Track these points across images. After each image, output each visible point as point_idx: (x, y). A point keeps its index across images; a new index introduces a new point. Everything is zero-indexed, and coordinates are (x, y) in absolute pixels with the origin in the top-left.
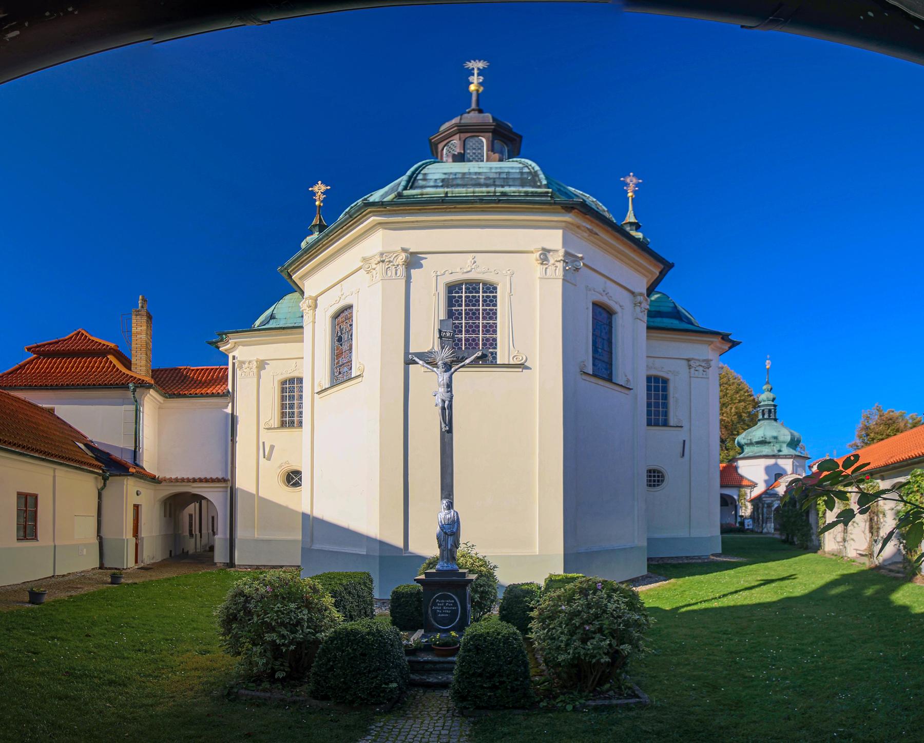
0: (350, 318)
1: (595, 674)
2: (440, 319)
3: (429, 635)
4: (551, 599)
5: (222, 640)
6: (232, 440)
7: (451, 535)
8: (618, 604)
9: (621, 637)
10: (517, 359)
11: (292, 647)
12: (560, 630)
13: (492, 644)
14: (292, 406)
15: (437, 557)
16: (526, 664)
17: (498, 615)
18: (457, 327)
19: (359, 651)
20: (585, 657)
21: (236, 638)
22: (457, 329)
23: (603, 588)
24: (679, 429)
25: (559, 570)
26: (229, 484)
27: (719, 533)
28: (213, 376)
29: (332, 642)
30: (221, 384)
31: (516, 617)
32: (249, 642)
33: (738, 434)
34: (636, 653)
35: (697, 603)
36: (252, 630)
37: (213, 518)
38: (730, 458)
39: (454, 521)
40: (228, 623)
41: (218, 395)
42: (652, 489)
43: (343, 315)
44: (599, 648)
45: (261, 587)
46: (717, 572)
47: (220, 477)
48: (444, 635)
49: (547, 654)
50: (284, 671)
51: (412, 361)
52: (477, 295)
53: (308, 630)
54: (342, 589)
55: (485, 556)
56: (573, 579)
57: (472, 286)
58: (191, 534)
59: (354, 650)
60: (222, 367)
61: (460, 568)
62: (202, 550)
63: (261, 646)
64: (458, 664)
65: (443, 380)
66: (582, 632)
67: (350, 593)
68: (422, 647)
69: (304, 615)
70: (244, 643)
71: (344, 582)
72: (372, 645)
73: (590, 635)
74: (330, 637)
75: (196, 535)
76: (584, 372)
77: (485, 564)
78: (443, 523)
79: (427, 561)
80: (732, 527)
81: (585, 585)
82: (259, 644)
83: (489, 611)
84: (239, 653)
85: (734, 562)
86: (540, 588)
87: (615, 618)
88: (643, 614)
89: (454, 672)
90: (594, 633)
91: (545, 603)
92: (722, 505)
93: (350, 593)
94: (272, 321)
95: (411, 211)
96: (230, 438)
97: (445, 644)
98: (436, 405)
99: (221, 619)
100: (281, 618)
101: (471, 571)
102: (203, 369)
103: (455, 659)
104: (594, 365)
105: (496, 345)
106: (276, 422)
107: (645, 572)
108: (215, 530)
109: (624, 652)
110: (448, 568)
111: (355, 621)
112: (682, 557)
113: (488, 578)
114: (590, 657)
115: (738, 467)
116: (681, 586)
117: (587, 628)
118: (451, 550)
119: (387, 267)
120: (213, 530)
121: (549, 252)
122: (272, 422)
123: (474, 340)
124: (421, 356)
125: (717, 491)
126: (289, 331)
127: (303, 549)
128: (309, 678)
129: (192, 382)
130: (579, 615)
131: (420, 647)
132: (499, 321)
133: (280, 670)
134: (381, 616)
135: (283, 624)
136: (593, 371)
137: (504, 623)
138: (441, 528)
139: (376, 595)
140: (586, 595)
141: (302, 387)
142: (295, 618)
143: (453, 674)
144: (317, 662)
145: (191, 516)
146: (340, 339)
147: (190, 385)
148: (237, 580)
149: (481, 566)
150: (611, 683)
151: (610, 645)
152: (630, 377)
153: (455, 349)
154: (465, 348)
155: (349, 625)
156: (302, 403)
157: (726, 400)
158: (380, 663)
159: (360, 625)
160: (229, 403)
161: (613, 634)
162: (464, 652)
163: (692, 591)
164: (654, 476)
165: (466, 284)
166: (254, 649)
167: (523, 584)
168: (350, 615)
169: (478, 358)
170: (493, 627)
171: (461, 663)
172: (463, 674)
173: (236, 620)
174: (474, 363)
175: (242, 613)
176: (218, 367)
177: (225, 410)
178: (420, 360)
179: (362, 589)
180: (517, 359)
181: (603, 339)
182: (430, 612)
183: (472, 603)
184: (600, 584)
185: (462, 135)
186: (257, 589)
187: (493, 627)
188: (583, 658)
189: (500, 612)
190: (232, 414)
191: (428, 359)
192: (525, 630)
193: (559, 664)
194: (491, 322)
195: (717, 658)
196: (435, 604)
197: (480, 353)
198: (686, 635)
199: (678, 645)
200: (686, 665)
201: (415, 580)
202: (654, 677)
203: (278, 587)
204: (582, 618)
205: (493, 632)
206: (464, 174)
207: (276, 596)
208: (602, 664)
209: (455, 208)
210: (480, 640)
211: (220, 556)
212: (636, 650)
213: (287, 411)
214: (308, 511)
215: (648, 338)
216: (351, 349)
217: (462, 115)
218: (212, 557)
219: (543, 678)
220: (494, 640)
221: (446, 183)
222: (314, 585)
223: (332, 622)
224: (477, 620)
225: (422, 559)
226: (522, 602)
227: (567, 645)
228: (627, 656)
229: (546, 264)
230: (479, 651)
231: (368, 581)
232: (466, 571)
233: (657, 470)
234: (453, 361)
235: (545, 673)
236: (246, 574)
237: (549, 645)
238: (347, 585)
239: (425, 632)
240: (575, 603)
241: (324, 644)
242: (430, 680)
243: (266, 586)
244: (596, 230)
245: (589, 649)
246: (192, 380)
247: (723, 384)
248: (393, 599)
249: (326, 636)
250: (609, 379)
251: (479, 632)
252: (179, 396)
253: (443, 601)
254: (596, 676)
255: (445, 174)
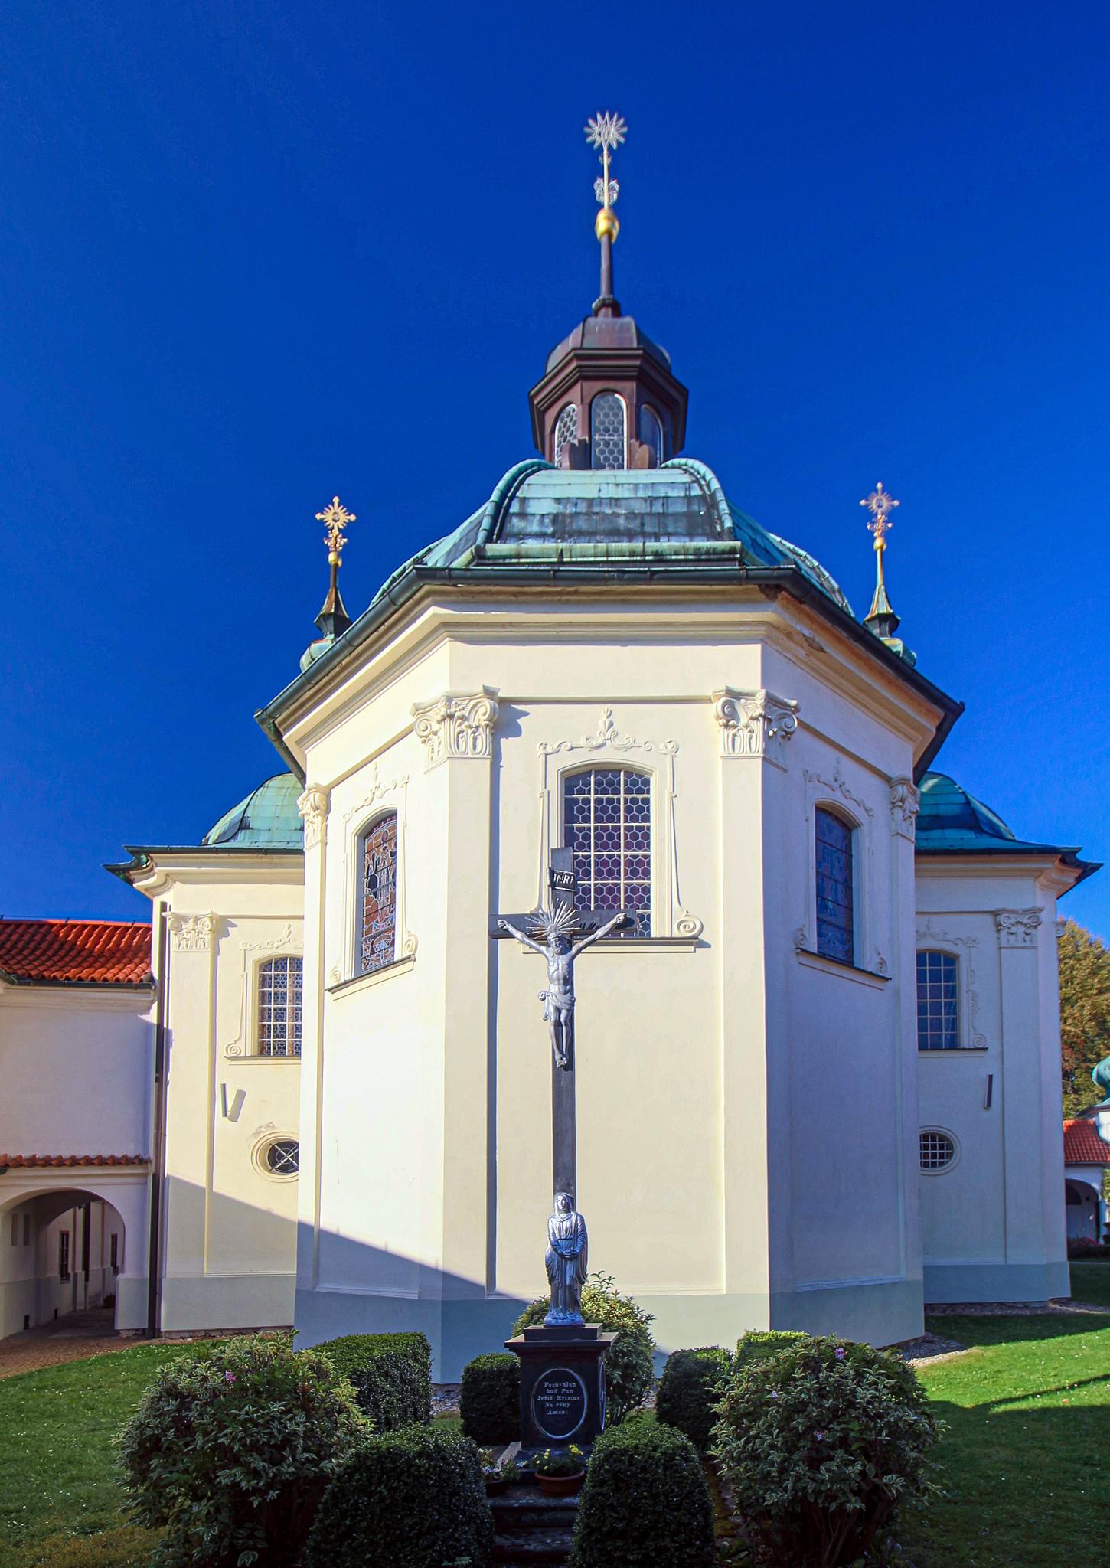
0: (390, 839)
1: (834, 1535)
2: (551, 847)
3: (530, 1453)
4: (752, 1377)
5: (128, 1497)
6: (157, 1080)
7: (571, 1259)
8: (877, 1389)
9: (882, 1456)
10: (685, 927)
11: (273, 1494)
12: (769, 1439)
13: (644, 1469)
14: (280, 1015)
15: (546, 1302)
16: (706, 1510)
17: (655, 1411)
18: (580, 864)
19: (402, 1491)
20: (815, 1499)
21: (158, 1486)
22: (581, 865)
23: (847, 1358)
24: (978, 1053)
25: (761, 1324)
26: (151, 1169)
27: (1065, 1258)
28: (118, 943)
29: (351, 1475)
30: (137, 960)
31: (687, 1416)
32: (186, 1495)
33: (1099, 1059)
34: (911, 1495)
35: (1025, 1397)
36: (193, 1467)
37: (114, 1238)
38: (1082, 1108)
39: (576, 1232)
40: (141, 1457)
41: (129, 985)
42: (930, 1171)
43: (378, 832)
44: (844, 1480)
45: (213, 1374)
46: (1063, 1335)
47: (131, 1154)
48: (557, 1453)
49: (745, 1489)
50: (255, 1548)
51: (502, 932)
52: (616, 796)
53: (306, 1455)
54: (372, 1367)
55: (632, 1298)
56: (790, 1342)
57: (607, 775)
58: (64, 1274)
59: (392, 1490)
60: (137, 925)
61: (587, 1321)
62: (88, 1307)
63: (210, 1499)
64: (582, 1511)
65: (558, 969)
66: (809, 1445)
67: (386, 1375)
68: (518, 1478)
69: (298, 1424)
70: (175, 1497)
71: (377, 1354)
72: (427, 1477)
73: (825, 1452)
74: (348, 1467)
75: (76, 1275)
76: (802, 949)
77: (631, 1312)
78: (557, 1237)
79: (529, 1309)
80: (1092, 1245)
81: (813, 1352)
82: (205, 1496)
83: (639, 1404)
84: (164, 1521)
85: (1098, 1316)
86: (729, 1358)
87: (872, 1419)
88: (924, 1413)
89: (575, 1529)
90: (832, 1447)
91: (741, 1386)
92: (1068, 1202)
93: (386, 1375)
94: (242, 834)
95: (500, 598)
96: (153, 1075)
97: (560, 1471)
98: (546, 1018)
99: (127, 1451)
100: (252, 1435)
101: (607, 1327)
102: (95, 927)
103: (577, 1500)
104: (820, 935)
105: (649, 899)
106: (249, 1046)
107: (920, 1331)
108: (119, 1264)
109: (891, 1491)
110: (565, 1322)
111: (395, 1431)
112: (991, 1304)
113: (636, 1338)
114: (825, 1500)
115: (1100, 1125)
116: (992, 1362)
117: (820, 1437)
118: (570, 1287)
119: (458, 729)
120: (114, 1264)
121: (739, 699)
122: (241, 1045)
123: (610, 891)
124: (518, 921)
125: (1058, 1175)
126: (276, 858)
127: (298, 1292)
128: (305, 1559)
129: (73, 953)
130: (803, 1411)
131: (514, 1479)
132: (653, 853)
133: (248, 1548)
134: (443, 1417)
135: (255, 1448)
136: (819, 948)
137: (665, 1427)
138: (553, 1246)
139: (436, 1377)
140: (816, 1371)
141: (300, 977)
142: (279, 1431)
143: (572, 1533)
144: (321, 1521)
145: (64, 1236)
146: (373, 883)
147: (67, 959)
148: (163, 1363)
149: (624, 1316)
150: (865, 1557)
151: (863, 1473)
152: (886, 957)
153: (578, 908)
154: (595, 907)
155: (385, 1440)
156: (300, 1010)
157: (1070, 991)
158: (440, 1514)
159: (403, 1439)
160: (152, 1002)
161: (867, 1451)
162: (594, 1487)
163: (1015, 1372)
164: (934, 1147)
165: (597, 773)
166: (195, 1509)
167: (699, 1351)
168: (387, 1418)
169: (618, 927)
170: (646, 1435)
171: (587, 1509)
172: (590, 1534)
173: (159, 1449)
174: (611, 938)
175: (171, 1435)
176: (129, 924)
177: (144, 1017)
178: (517, 929)
179: (409, 1365)
180: (685, 927)
181: (836, 881)
182: (532, 1406)
183: (608, 1388)
184: (841, 1350)
185: (587, 385)
186: (205, 1379)
187: (646, 1435)
188: (812, 1500)
189: (659, 1404)
190: (160, 1025)
191: (529, 927)
192: (703, 1440)
193: (766, 1514)
194: (640, 853)
195: (1076, 1516)
196: (541, 1391)
197: (619, 918)
198: (1006, 1462)
199: (993, 1483)
200: (1013, 1526)
201: (507, 1345)
202: (950, 1550)
203: (247, 1371)
204: (808, 1418)
205: (646, 1445)
206: (590, 502)
207: (245, 1389)
208: (849, 1515)
209: (576, 593)
210: (620, 1461)
211: (128, 1316)
212: (912, 1489)
213: (272, 1023)
214: (309, 1219)
215: (918, 874)
216: (393, 903)
217: (585, 321)
218: (112, 1320)
219: (737, 1542)
220: (646, 1461)
221: (561, 526)
222: (320, 1362)
223: (351, 1434)
224: (617, 1421)
225: (518, 1304)
226: (697, 1385)
227: (783, 1471)
228: (895, 1500)
229: (735, 727)
230: (620, 1484)
231: (420, 1351)
232: (598, 1325)
233: (940, 1136)
234: (574, 933)
235: (741, 1531)
236: (182, 1349)
237: (750, 1470)
238: (383, 1360)
239: (523, 1447)
240: (796, 1387)
241: (334, 1482)
242: (531, 1547)
243: (223, 1370)
244: (821, 640)
245: (823, 1481)
246: (88, 956)
247: (1065, 958)
248: (466, 1383)
249: (339, 1465)
250: (848, 962)
251: (620, 1445)
252: (41, 981)
253: (557, 1385)
254: (837, 1540)
255: (558, 501)
